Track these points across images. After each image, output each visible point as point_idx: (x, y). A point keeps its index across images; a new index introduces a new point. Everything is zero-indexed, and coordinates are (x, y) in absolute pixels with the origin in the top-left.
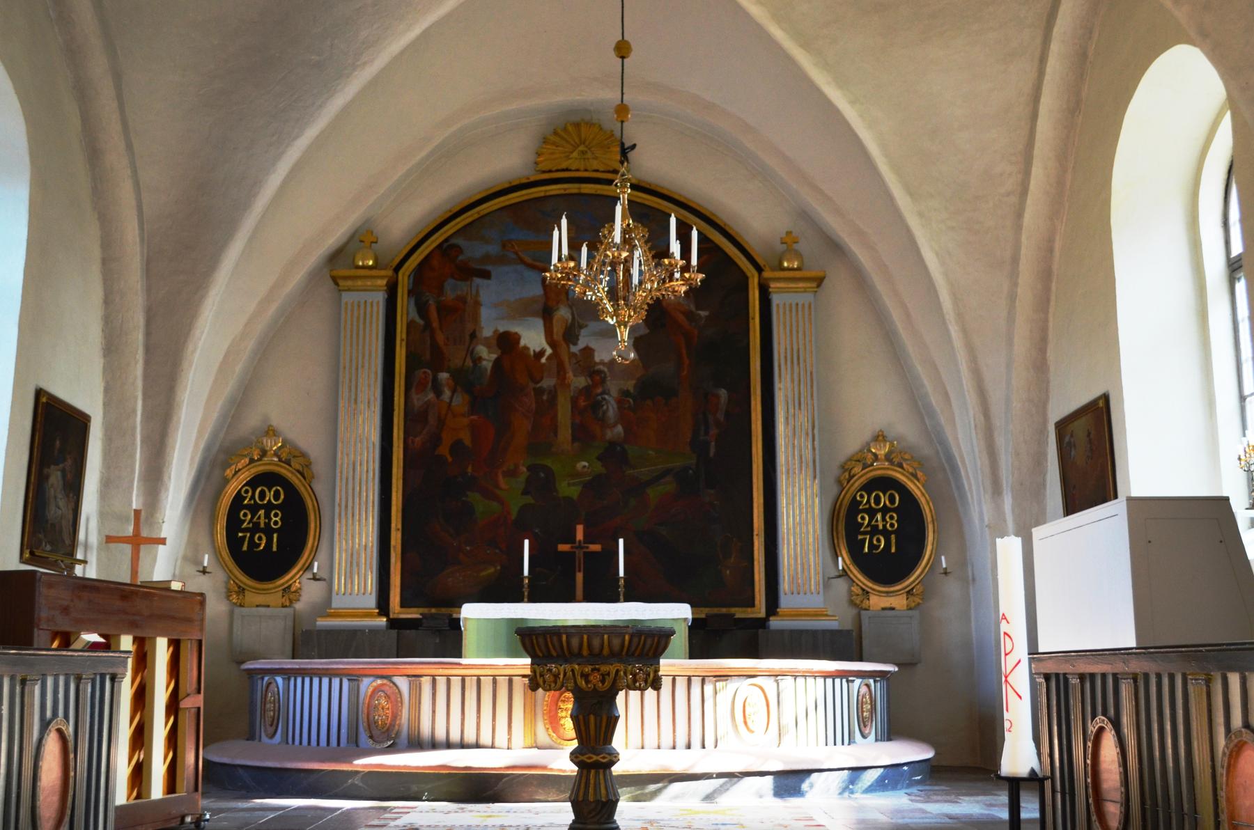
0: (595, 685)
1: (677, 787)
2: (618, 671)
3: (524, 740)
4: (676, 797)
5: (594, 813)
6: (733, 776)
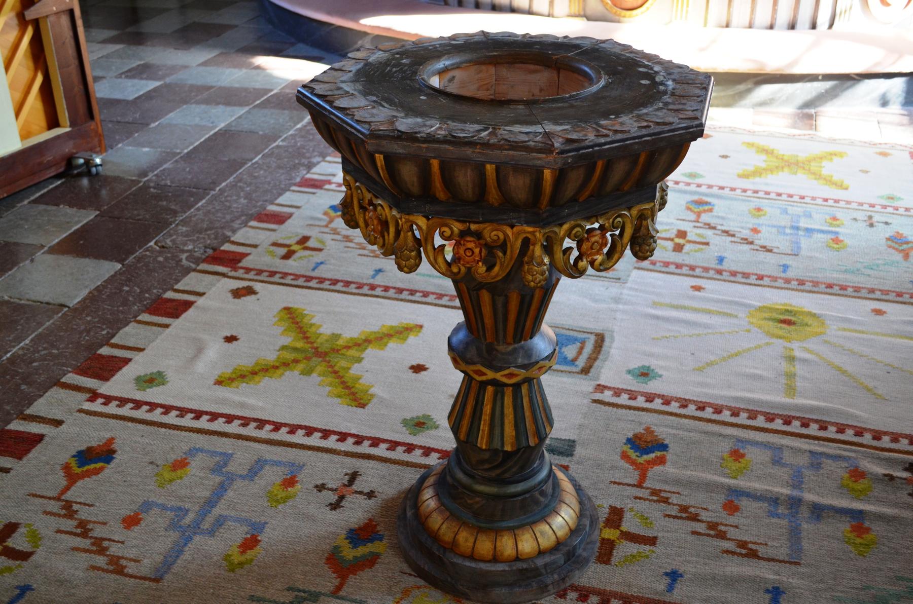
0: (469, 269)
1: (767, 90)
2: (526, 243)
3: (570, 6)
4: (763, 104)
5: (486, 466)
6: (847, 80)
